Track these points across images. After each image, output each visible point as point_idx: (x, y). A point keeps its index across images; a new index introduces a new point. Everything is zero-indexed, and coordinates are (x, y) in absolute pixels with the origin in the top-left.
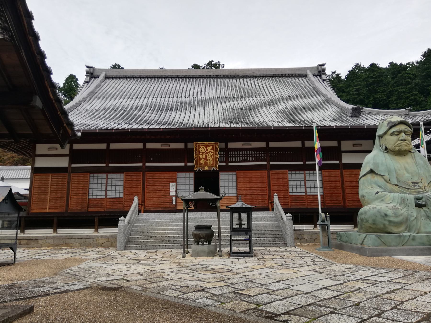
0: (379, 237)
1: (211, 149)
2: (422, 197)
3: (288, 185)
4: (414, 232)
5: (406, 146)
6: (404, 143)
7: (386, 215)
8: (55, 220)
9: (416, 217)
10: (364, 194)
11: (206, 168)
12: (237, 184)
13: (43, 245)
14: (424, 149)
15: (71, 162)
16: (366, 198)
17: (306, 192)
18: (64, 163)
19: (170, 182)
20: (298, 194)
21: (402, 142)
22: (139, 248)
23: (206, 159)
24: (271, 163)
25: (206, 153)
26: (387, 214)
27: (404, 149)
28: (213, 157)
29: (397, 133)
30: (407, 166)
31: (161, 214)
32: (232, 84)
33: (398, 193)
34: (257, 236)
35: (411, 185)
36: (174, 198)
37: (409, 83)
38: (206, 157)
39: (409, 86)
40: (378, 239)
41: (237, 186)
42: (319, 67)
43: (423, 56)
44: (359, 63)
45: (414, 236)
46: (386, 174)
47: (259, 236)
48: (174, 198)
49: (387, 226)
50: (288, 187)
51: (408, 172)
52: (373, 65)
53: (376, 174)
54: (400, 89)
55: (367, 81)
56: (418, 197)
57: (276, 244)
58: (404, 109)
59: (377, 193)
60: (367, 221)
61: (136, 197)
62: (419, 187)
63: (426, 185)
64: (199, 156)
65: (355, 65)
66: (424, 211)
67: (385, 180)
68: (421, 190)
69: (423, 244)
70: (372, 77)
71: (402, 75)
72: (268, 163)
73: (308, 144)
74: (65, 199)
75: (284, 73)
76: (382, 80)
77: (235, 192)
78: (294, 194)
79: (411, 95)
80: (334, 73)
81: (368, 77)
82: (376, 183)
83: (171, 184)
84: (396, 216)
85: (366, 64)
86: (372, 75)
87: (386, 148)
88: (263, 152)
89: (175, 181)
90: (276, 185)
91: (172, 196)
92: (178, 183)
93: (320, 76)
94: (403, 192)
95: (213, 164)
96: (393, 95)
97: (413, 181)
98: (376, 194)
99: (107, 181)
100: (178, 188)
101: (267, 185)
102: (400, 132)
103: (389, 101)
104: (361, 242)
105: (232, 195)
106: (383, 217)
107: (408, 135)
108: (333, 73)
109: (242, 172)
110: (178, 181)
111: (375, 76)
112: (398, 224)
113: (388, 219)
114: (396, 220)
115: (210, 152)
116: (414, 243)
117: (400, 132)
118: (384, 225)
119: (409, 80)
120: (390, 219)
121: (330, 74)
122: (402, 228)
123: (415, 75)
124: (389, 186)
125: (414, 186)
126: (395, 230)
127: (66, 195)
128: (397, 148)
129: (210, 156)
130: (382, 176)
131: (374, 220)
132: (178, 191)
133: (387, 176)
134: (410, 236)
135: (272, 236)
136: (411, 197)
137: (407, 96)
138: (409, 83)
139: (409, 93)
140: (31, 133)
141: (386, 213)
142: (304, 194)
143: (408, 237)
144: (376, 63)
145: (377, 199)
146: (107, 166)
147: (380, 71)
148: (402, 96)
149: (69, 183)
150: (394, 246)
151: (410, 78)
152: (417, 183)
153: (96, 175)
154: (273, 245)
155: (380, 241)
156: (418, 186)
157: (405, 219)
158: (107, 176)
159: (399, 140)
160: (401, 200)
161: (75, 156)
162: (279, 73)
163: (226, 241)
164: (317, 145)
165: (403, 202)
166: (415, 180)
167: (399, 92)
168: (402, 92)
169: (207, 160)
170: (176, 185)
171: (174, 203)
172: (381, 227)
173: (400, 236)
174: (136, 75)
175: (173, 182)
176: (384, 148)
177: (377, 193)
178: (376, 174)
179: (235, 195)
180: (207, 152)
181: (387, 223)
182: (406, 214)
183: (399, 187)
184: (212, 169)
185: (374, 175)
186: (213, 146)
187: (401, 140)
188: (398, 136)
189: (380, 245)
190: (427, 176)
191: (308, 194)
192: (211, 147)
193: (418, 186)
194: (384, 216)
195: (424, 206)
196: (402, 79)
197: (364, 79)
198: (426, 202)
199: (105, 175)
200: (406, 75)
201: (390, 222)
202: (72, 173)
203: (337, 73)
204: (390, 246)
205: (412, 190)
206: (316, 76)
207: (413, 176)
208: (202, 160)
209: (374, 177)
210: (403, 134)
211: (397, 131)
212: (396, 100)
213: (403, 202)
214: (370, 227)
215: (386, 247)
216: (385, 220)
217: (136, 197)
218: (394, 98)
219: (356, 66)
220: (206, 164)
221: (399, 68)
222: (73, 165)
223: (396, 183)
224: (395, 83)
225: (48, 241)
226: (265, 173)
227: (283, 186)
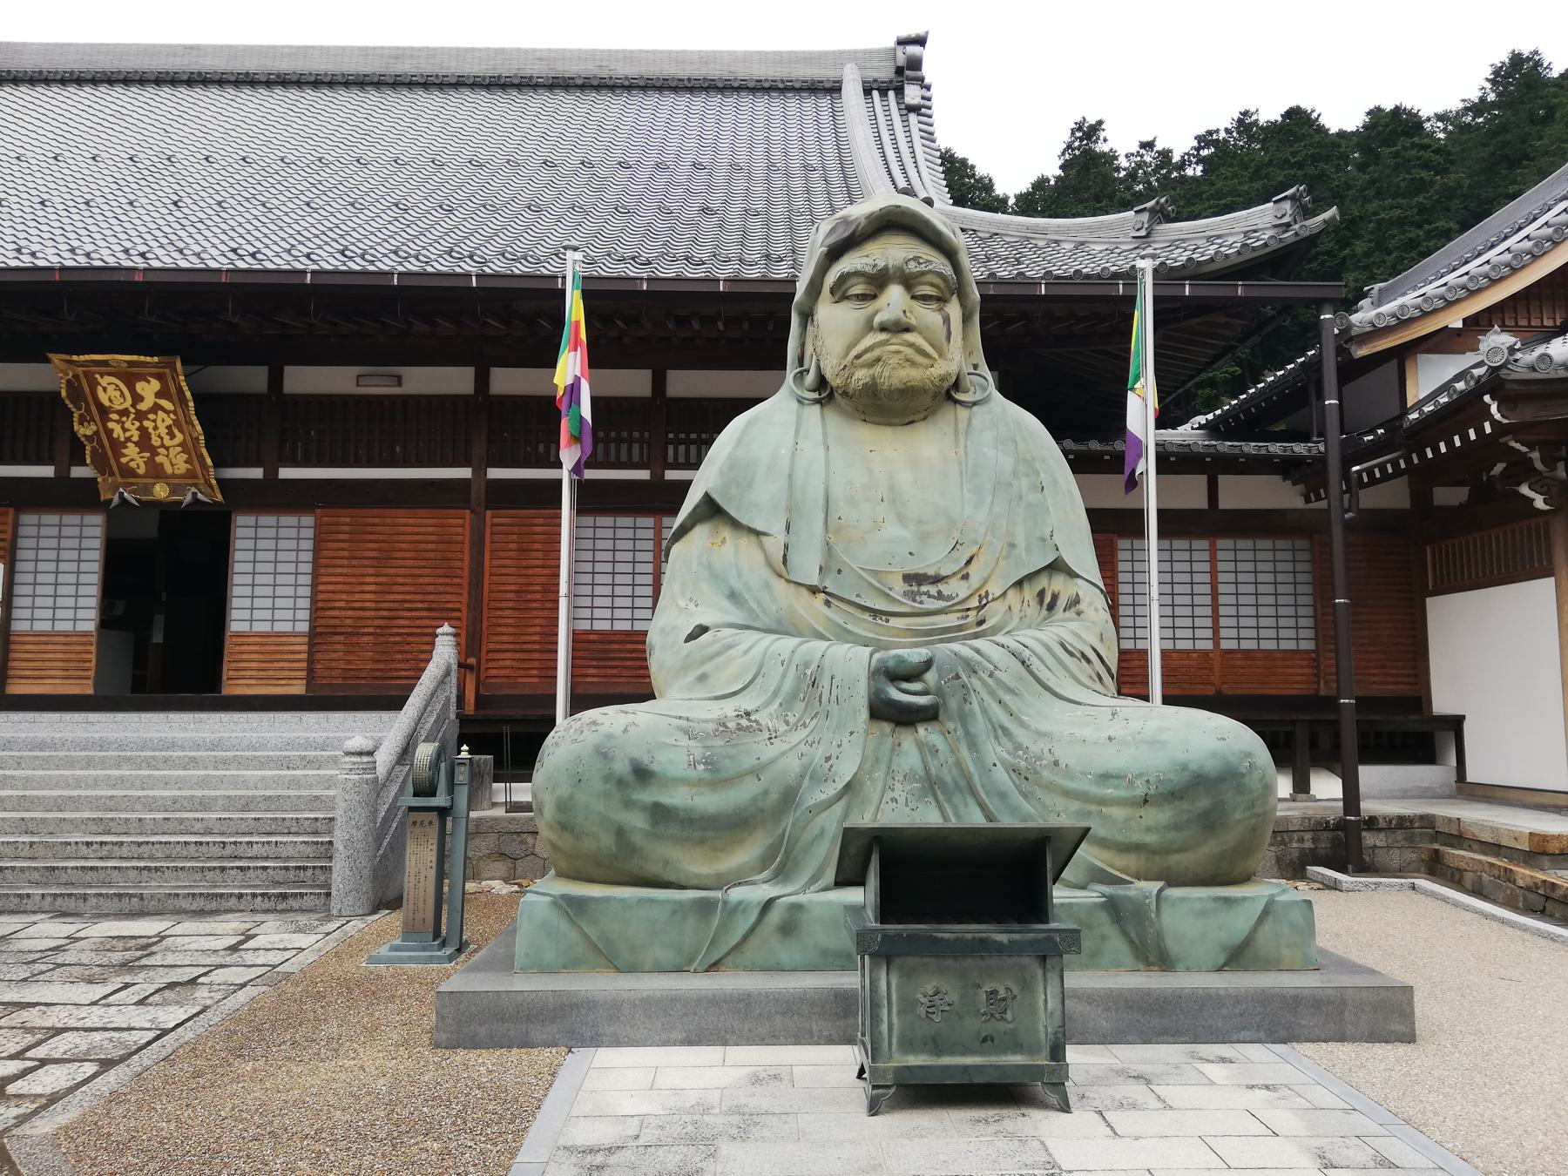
1: (158, 395)
2: (928, 664)
4: (814, 879)
5: (913, 364)
6: (896, 344)
7: (642, 774)
9: (848, 787)
11: (161, 492)
12: (315, 575)
14: (1144, 400)
17: (1216, 638)
20: (619, 626)
21: (884, 336)
23: (144, 442)
24: (494, 473)
25: (141, 416)
26: (655, 767)
27: (896, 383)
28: (179, 437)
29: (858, 289)
30: (905, 478)
33: (822, 637)
34: (229, 851)
35: (899, 587)
37: (1420, 186)
38: (143, 431)
39: (1420, 199)
40: (564, 926)
41: (314, 585)
42: (900, 49)
43: (1493, 82)
44: (1253, 110)
45: (797, 908)
47: (240, 851)
49: (638, 840)
51: (901, 519)
52: (1296, 116)
53: (736, 525)
54: (1384, 209)
55: (1267, 176)
56: (901, 660)
57: (284, 896)
58: (1132, 213)
61: (446, 628)
62: (942, 604)
63: (995, 589)
64: (109, 432)
65: (1236, 116)
66: (921, 746)
68: (951, 620)
70: (1286, 161)
71: (1396, 155)
72: (479, 471)
73: (634, 383)
75: (743, 72)
76: (1323, 173)
78: (598, 626)
79: (1428, 233)
80: (1147, 145)
81: (1270, 163)
84: (717, 779)
85: (1270, 112)
86: (1286, 153)
87: (822, 383)
88: (636, 435)
90: (511, 579)
93: (900, 91)
95: (190, 474)
96: (1358, 237)
97: (915, 567)
98: (692, 637)
101: (465, 582)
102: (878, 281)
103: (1344, 258)
105: (287, 627)
106: (621, 783)
107: (925, 298)
108: (1144, 145)
109: (345, 518)
111: (1298, 158)
113: (647, 796)
114: (709, 802)
115: (156, 408)
116: (786, 952)
117: (878, 281)
118: (620, 833)
119: (1424, 174)
120: (666, 800)
121: (1135, 148)
122: (745, 854)
123: (1449, 153)
125: (912, 596)
126: (697, 864)
128: (862, 376)
129: (163, 431)
130: (758, 534)
134: (768, 905)
135: (308, 850)
136: (851, 663)
137: (1411, 240)
138: (1420, 186)
139: (1420, 227)
141: (646, 760)
142: (1208, 645)
143: (754, 916)
144: (1306, 105)
147: (1317, 138)
148: (1393, 237)
150: (660, 969)
151: (1426, 166)
152: (938, 579)
154: (267, 905)
155: (574, 936)
156: (940, 596)
157: (774, 796)
158: (1213, 551)
159: (869, 327)
160: (801, 677)
162: (715, 72)
163: (36, 876)
164: (569, 366)
165: (809, 687)
166: (933, 560)
167: (1379, 222)
168: (1391, 222)
169: (154, 451)
174: (61, 68)
176: (810, 378)
178: (736, 525)
179: (303, 627)
180: (143, 406)
181: (637, 821)
182: (792, 765)
184: (189, 498)
185: (726, 532)
186: (160, 377)
187: (883, 328)
188: (871, 307)
189: (573, 964)
190: (1020, 541)
192: (155, 385)
193: (940, 596)
194: (630, 778)
195: (929, 715)
196: (1397, 166)
197: (1258, 170)
198: (939, 692)
200: (1414, 152)
201: (660, 814)
203: (1159, 147)
204: (633, 969)
205: (895, 622)
206: (883, 93)
207: (924, 537)
208: (131, 451)
209: (724, 541)
210: (895, 294)
211: (857, 274)
212: (1367, 254)
213: (809, 687)
216: (629, 805)
217: (446, 628)
218: (1360, 247)
219: (1240, 121)
220: (156, 472)
221: (1387, 125)
223: (814, 580)
224: (1373, 182)
226: (459, 523)
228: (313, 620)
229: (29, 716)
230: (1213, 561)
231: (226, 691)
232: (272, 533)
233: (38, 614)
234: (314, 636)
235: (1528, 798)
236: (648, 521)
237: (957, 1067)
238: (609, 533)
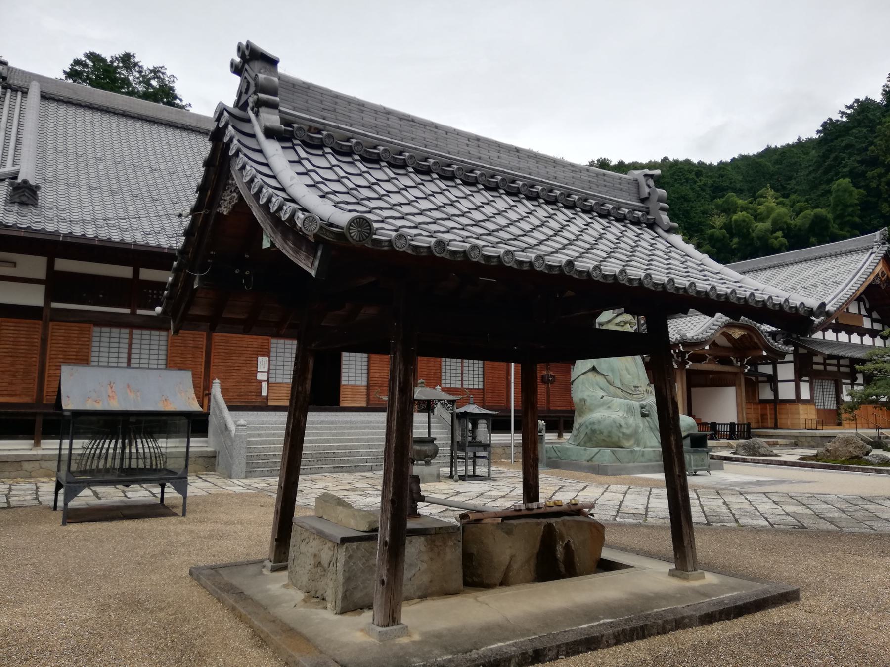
0: (613, 452)
3: (441, 372)
8: (39, 421)
10: (586, 398)
12: (369, 366)
13: (33, 474)
15: (50, 296)
16: (588, 403)
17: (462, 384)
18: (34, 297)
19: (258, 355)
22: (266, 473)
31: (330, 413)
32: (139, 131)
36: (264, 385)
46: (610, 374)
48: (264, 385)
50: (441, 375)
51: (629, 374)
59: (602, 397)
60: (601, 433)
61: (217, 381)
67: (608, 382)
69: (650, 461)
74: (36, 375)
77: (366, 379)
82: (598, 384)
83: (260, 358)
89: (267, 354)
91: (261, 382)
92: (272, 358)
94: (626, 398)
99: (130, 345)
100: (271, 367)
104: (588, 458)
110: (272, 354)
112: (628, 437)
122: (632, 442)
124: (611, 388)
127: (37, 367)
131: (610, 432)
132: (271, 371)
133: (610, 377)
136: (636, 404)
140: (313, 273)
142: (460, 386)
145: (602, 405)
146: (133, 313)
149: (44, 341)
153: (107, 329)
158: (131, 334)
161: (58, 285)
170: (269, 361)
171: (264, 393)
172: (601, 438)
173: (632, 451)
175: (263, 355)
177: (602, 397)
179: (365, 383)
181: (621, 435)
183: (622, 391)
191: (465, 386)
199: (127, 331)
201: (623, 434)
202: (52, 320)
214: (604, 440)
215: (619, 464)
217: (217, 381)
222: (55, 305)
225: (45, 464)
227: (435, 373)
228: (368, 381)
229: (376, 413)
230: (462, 366)
231: (342, 405)
232: (117, 336)
233: (278, 376)
234: (368, 387)
235: (126, 512)
236: (459, 360)
237: (654, 480)
238: (148, 337)
